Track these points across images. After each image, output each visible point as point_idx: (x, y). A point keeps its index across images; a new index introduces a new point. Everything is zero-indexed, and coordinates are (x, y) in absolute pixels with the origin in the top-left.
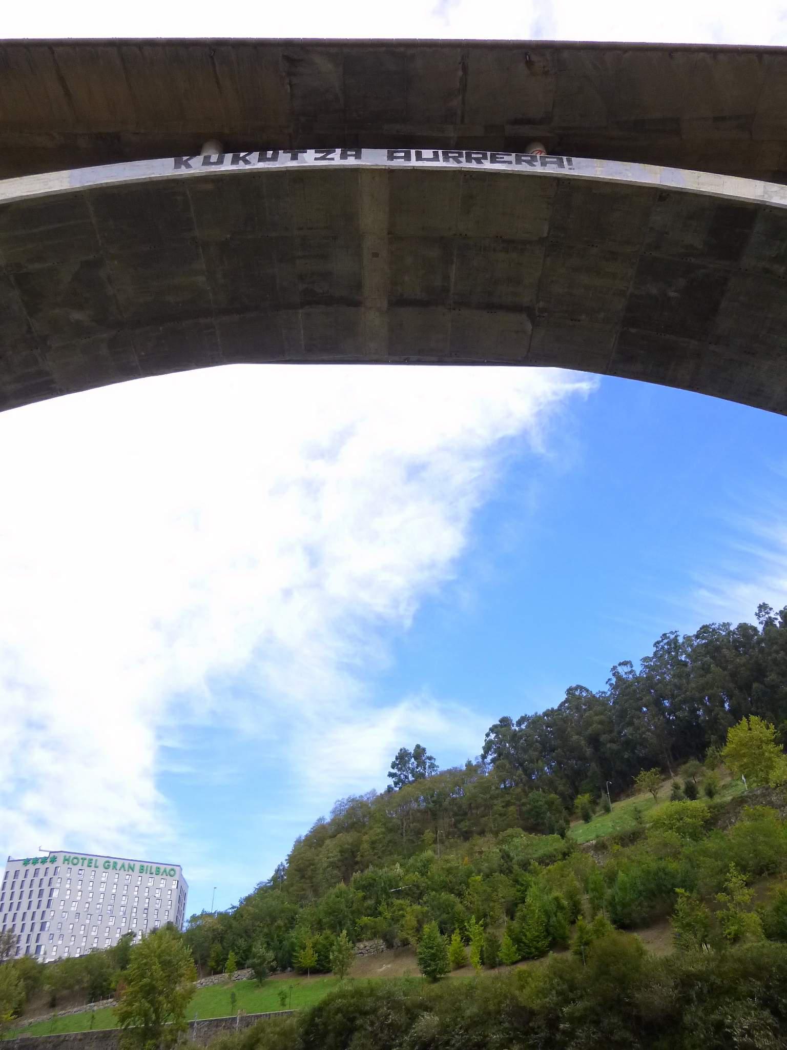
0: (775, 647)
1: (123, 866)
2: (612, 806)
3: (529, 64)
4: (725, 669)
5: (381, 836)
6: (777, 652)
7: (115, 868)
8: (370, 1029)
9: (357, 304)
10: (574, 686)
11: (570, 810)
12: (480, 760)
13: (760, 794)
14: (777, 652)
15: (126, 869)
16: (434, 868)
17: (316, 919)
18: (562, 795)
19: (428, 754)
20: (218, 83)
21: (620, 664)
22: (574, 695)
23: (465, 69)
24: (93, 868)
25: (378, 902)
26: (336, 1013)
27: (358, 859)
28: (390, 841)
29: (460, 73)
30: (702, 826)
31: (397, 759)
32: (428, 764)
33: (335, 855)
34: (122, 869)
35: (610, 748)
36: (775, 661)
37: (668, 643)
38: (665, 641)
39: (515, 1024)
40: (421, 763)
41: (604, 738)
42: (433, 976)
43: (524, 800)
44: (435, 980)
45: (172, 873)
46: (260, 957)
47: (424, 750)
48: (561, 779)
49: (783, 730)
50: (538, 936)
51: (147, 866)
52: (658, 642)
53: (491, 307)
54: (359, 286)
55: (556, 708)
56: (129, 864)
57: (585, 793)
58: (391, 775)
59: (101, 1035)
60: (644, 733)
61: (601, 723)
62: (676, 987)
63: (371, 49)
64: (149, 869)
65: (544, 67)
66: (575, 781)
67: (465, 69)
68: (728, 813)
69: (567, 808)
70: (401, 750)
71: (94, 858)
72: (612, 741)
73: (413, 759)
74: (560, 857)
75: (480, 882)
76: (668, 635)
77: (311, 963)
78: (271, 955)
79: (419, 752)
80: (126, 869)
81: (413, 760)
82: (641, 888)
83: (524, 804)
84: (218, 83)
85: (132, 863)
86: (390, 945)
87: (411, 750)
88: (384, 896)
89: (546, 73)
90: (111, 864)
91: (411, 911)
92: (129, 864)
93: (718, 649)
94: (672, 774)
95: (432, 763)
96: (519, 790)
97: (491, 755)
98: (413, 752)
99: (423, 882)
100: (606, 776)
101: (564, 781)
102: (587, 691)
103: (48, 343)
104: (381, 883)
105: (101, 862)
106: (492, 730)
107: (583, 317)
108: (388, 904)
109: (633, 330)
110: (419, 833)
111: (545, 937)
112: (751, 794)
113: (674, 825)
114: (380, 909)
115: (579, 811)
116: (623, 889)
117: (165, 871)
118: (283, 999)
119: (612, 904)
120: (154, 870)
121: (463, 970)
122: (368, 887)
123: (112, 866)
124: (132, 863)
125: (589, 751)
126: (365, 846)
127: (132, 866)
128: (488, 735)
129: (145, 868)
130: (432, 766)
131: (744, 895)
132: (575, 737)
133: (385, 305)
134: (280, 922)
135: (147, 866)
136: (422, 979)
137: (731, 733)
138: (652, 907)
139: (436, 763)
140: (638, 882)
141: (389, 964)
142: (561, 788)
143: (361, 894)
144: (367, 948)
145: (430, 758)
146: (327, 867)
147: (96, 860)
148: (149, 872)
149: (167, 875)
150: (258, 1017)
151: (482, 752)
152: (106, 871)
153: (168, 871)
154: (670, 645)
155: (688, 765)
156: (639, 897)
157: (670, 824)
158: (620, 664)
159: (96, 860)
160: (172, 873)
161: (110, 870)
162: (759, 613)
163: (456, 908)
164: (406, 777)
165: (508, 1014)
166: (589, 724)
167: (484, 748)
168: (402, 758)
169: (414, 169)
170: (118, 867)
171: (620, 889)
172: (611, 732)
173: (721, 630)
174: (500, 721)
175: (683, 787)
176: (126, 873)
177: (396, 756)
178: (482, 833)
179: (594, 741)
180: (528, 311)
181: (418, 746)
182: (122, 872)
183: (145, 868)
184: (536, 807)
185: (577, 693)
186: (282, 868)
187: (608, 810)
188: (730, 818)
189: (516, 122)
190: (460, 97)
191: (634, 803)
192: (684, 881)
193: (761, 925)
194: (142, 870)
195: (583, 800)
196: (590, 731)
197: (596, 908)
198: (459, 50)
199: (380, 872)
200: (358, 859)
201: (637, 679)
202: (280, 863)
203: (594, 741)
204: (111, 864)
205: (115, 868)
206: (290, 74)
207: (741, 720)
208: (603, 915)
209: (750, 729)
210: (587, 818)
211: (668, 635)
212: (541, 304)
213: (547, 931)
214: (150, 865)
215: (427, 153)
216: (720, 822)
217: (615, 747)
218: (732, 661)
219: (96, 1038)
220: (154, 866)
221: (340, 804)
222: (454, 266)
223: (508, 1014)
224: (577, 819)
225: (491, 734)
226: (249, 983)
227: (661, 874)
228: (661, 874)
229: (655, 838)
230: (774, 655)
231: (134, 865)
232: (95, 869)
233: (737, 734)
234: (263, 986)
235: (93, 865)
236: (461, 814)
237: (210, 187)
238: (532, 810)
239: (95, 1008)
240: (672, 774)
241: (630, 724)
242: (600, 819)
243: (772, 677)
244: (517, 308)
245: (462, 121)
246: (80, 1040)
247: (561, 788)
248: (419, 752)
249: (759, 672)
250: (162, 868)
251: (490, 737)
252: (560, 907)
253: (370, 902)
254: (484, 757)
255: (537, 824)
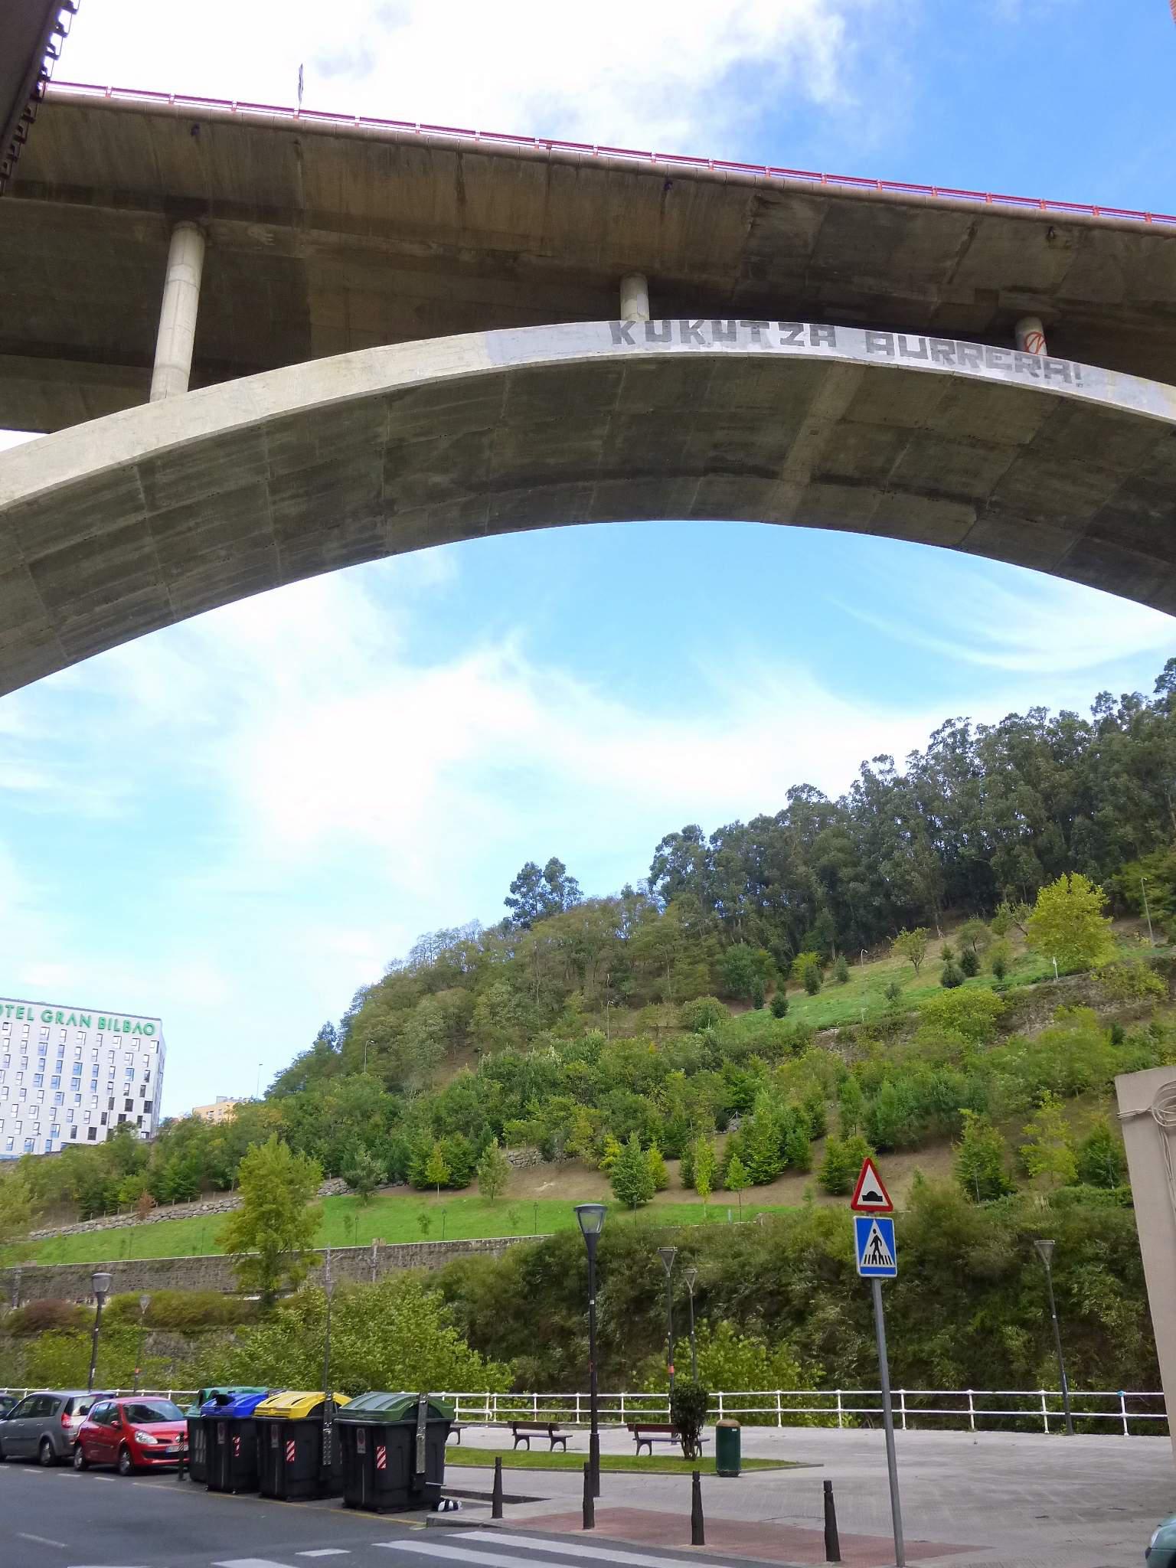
0: (1116, 767)
1: (73, 1018)
2: (851, 970)
3: (1050, 237)
4: (1035, 786)
5: (506, 996)
6: (1117, 775)
7: (59, 1021)
8: (627, 1273)
9: (771, 475)
10: (800, 784)
11: (785, 971)
12: (646, 886)
13: (1074, 986)
14: (1117, 775)
15: (78, 1023)
16: (606, 1055)
17: (431, 1117)
18: (776, 952)
19: (568, 874)
20: (662, 213)
21: (875, 760)
22: (798, 798)
23: (972, 233)
24: (25, 1021)
25: (526, 1098)
26: (579, 1256)
27: (471, 1028)
28: (518, 1005)
29: (965, 237)
30: (992, 1024)
31: (519, 878)
32: (567, 889)
33: (437, 1024)
34: (72, 1023)
35: (854, 889)
36: (1114, 790)
37: (953, 735)
38: (949, 730)
39: (818, 1272)
40: (557, 888)
41: (845, 872)
42: (631, 1201)
43: (717, 957)
44: (632, 1207)
45: (149, 1030)
46: (364, 1169)
47: (563, 867)
48: (776, 927)
49: (1109, 888)
50: (770, 1157)
51: (110, 1020)
52: (938, 732)
53: (933, 494)
54: (781, 456)
55: (773, 816)
56: (82, 1016)
57: (810, 950)
58: (509, 902)
59: (157, 1266)
60: (908, 872)
61: (840, 850)
62: (1013, 1244)
63: (867, 204)
64: (113, 1023)
65: (1067, 242)
66: (796, 933)
67: (972, 233)
68: (1028, 1006)
69: (780, 970)
70: (527, 865)
71: (27, 1006)
72: (856, 878)
73: (543, 879)
74: (788, 1049)
75: (682, 1080)
76: (953, 722)
77: (442, 1177)
78: (379, 1165)
79: (555, 869)
80: (78, 1023)
81: (543, 881)
82: (913, 1104)
83: (719, 962)
84: (662, 213)
85: (86, 1014)
86: (547, 1155)
87: (542, 865)
88: (534, 1090)
89: (1067, 248)
90: (54, 1015)
91: (583, 1117)
92: (82, 1016)
93: (1028, 755)
94: (940, 933)
95: (572, 888)
96: (712, 941)
97: (662, 879)
98: (544, 869)
99: (592, 1073)
100: (843, 928)
101: (779, 930)
102: (820, 794)
103: (395, 508)
104: (530, 1074)
105: (37, 1011)
106: (666, 841)
107: (1042, 518)
108: (540, 1101)
109: (1097, 541)
110: (561, 995)
111: (779, 1158)
112: (1061, 984)
113: (955, 1019)
114: (530, 1107)
115: (799, 977)
116: (890, 1104)
117: (138, 1027)
118: (426, 1226)
119: (871, 1120)
120: (120, 1026)
121: (664, 1194)
122: (506, 1076)
123: (55, 1017)
124: (86, 1014)
125: (820, 891)
126: (482, 1011)
127: (87, 1019)
128: (659, 849)
129: (107, 1023)
130: (573, 892)
131: (1058, 1128)
132: (802, 869)
133: (807, 480)
134: (377, 1119)
135: (110, 1020)
136: (618, 1205)
137: (1043, 894)
138: (925, 1128)
139: (580, 888)
140: (910, 1095)
141: (551, 1181)
142: (774, 941)
143: (498, 1086)
144: (512, 1158)
145: (571, 880)
146: (427, 1039)
147: (30, 1010)
148: (112, 1028)
149: (141, 1033)
150: (403, 1247)
151: (649, 874)
152: (46, 1025)
153: (142, 1027)
154: (955, 738)
155: (967, 925)
156: (909, 1115)
157: (950, 1018)
158: (875, 760)
159: (30, 1010)
160: (149, 1030)
161: (52, 1024)
162: (1096, 707)
163: (648, 1113)
164: (533, 907)
165: (812, 1263)
166: (824, 850)
167: (652, 868)
168: (527, 878)
169: (898, 369)
170: (65, 1020)
171: (885, 1103)
172: (855, 865)
173: (1033, 717)
174: (684, 831)
175: (958, 955)
176: (78, 1028)
177: (519, 875)
178: (657, 999)
179: (829, 876)
180: (978, 503)
181: (554, 862)
182: (71, 1028)
183: (107, 1023)
184: (737, 968)
185: (804, 796)
186: (328, 1030)
187: (844, 979)
188: (1029, 1014)
189: (1014, 289)
190: (956, 260)
191: (883, 972)
192: (972, 1099)
193: (1074, 1163)
194: (102, 1025)
195: (805, 960)
196: (824, 860)
197: (847, 1123)
198: (972, 215)
199: (526, 1057)
200: (471, 1028)
201: (898, 782)
202: (326, 1023)
203: (829, 876)
204: (54, 1015)
205: (59, 1021)
206: (756, 215)
207: (1059, 878)
208: (858, 1136)
209: (1069, 892)
210: (812, 989)
211: (953, 722)
212: (994, 499)
213: (781, 1149)
214: (115, 1017)
215: (913, 341)
216: (1014, 1017)
217: (863, 888)
218: (1048, 777)
219: (149, 1269)
220: (122, 1019)
221: (425, 941)
222: (905, 452)
223: (812, 1263)
224: (795, 986)
225: (664, 848)
226: (346, 1200)
227: (942, 1088)
228: (942, 1088)
229: (929, 1035)
230: (1113, 780)
231: (89, 1017)
232: (29, 1023)
233: (1052, 896)
234: (369, 1204)
235: (25, 1016)
236: (621, 969)
237: (653, 367)
238: (732, 971)
239: (99, 1227)
240: (940, 933)
241: (888, 856)
242: (831, 991)
243: (1108, 811)
244: (964, 499)
245: (950, 282)
246: (124, 1271)
247: (774, 941)
248: (555, 869)
249: (1086, 798)
250: (134, 1022)
251: (661, 852)
252: (800, 1121)
253: (515, 1097)
254: (652, 882)
255: (738, 992)
